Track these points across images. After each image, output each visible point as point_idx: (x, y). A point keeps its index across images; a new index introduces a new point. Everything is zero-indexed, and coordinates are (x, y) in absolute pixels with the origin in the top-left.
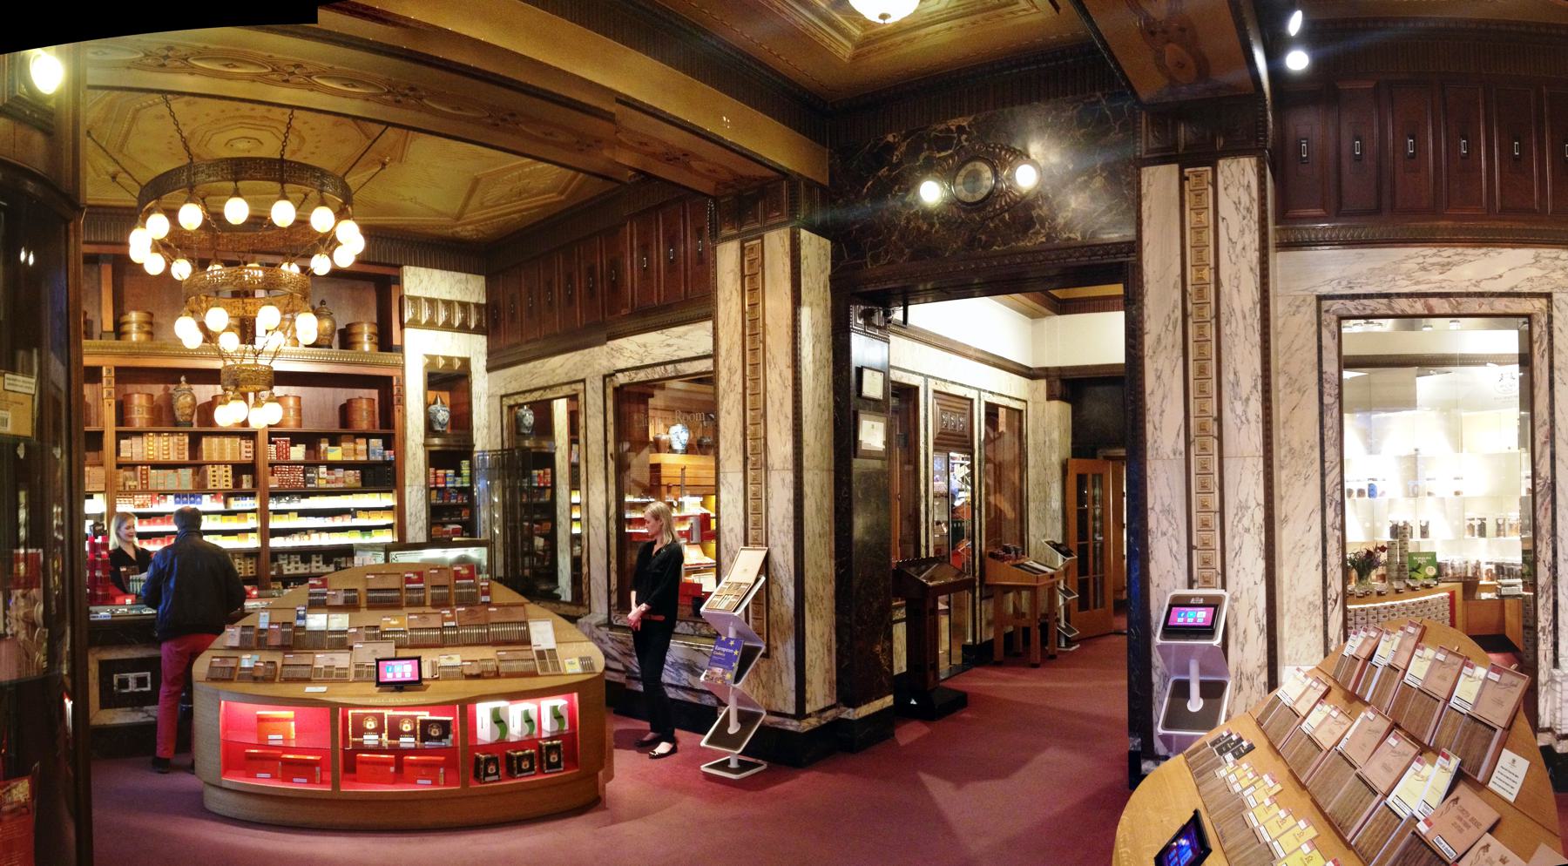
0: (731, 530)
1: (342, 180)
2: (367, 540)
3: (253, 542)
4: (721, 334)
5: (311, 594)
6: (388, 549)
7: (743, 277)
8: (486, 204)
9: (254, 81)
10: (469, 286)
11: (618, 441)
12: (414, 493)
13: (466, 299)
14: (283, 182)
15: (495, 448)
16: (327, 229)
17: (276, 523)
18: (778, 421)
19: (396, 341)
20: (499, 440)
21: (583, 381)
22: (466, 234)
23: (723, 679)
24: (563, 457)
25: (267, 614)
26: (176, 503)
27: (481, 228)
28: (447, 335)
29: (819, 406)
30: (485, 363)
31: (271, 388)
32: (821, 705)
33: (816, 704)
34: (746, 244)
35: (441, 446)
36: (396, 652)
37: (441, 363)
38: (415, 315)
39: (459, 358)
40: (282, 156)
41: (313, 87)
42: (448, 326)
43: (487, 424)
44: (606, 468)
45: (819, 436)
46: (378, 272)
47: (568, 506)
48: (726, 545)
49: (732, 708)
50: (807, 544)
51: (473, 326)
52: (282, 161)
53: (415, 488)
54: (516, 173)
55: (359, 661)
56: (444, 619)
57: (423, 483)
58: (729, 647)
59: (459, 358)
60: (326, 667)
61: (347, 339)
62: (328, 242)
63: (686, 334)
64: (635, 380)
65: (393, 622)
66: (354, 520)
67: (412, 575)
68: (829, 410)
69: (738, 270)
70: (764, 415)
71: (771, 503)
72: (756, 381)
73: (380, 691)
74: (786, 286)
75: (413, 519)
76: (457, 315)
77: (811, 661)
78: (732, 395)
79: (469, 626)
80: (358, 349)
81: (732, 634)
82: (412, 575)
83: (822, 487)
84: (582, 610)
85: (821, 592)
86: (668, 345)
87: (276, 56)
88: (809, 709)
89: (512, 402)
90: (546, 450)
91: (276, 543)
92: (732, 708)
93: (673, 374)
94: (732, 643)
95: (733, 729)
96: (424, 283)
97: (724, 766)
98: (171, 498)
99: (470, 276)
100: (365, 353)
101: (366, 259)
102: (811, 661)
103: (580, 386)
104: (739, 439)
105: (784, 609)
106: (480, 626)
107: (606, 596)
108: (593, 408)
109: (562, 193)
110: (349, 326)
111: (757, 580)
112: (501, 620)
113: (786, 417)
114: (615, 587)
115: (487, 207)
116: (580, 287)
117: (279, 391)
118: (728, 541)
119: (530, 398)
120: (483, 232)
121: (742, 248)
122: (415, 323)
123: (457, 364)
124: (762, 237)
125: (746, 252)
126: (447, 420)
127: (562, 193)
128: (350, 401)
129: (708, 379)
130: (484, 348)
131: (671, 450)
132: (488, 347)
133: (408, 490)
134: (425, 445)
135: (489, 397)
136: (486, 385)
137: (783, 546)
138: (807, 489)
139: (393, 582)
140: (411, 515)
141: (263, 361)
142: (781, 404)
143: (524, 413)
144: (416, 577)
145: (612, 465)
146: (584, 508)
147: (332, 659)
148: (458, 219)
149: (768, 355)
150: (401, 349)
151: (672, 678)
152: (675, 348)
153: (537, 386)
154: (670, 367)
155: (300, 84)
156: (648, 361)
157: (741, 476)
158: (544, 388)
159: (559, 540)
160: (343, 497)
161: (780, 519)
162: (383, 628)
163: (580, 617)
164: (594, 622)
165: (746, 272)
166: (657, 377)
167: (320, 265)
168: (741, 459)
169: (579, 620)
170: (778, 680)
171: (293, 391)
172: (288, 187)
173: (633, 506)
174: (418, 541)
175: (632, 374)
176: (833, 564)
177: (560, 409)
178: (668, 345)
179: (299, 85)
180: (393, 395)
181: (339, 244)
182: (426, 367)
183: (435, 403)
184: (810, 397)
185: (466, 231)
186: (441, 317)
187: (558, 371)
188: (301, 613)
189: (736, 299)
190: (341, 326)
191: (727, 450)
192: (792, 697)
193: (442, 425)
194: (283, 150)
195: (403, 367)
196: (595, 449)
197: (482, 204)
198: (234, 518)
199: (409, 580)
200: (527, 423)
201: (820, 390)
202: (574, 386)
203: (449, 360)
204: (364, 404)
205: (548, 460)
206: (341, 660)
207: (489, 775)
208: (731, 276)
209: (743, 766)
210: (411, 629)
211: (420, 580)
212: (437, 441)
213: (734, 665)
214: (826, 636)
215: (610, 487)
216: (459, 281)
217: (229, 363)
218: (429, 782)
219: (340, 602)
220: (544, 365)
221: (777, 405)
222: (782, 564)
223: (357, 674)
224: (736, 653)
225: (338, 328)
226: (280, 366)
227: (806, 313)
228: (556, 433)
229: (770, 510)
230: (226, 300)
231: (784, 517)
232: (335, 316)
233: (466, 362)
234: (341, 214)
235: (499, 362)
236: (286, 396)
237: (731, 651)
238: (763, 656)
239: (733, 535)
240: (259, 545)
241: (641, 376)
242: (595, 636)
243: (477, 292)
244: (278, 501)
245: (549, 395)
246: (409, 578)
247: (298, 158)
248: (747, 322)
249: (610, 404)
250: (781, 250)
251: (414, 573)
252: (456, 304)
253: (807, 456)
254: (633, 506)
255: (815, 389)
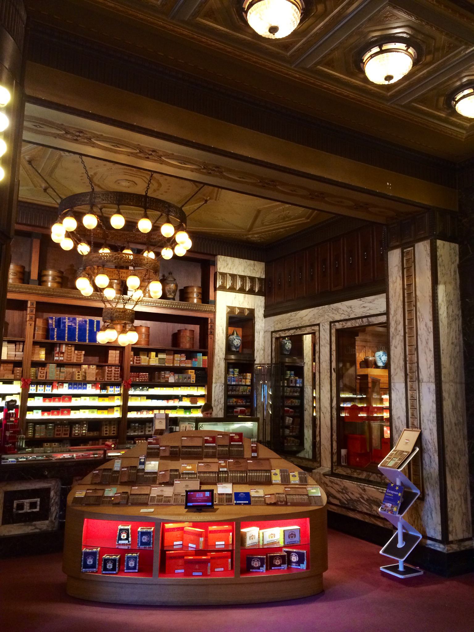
0: (399, 418)
1: (180, 209)
2: (188, 415)
3: (117, 414)
4: (391, 302)
5: (148, 448)
6: (197, 420)
7: (403, 269)
8: (265, 223)
9: (129, 156)
10: (256, 268)
11: (338, 361)
12: (217, 388)
13: (253, 275)
14: (146, 208)
15: (267, 362)
16: (170, 235)
17: (132, 403)
18: (425, 353)
19: (211, 298)
20: (270, 358)
21: (318, 325)
22: (254, 239)
23: (392, 511)
24: (309, 369)
25: (120, 461)
26: (69, 388)
27: (262, 236)
28: (241, 296)
29: (452, 343)
30: (263, 313)
31: (133, 322)
32: (460, 536)
33: (456, 535)
34: (405, 250)
35: (235, 360)
36: (200, 487)
37: (237, 311)
38: (223, 283)
39: (248, 309)
40: (146, 194)
41: (162, 162)
42: (242, 290)
43: (263, 348)
44: (331, 377)
45: (452, 363)
46: (203, 258)
47: (311, 399)
48: (396, 427)
49: (400, 532)
50: (446, 429)
51: (257, 290)
52: (146, 196)
53: (218, 384)
54: (281, 208)
55: (176, 492)
56: (220, 466)
57: (223, 382)
58: (395, 491)
59: (248, 309)
60: (158, 496)
61: (184, 295)
62: (171, 242)
63: (374, 300)
64: (345, 327)
65: (188, 467)
66: (180, 402)
67: (208, 438)
68: (460, 346)
69: (400, 265)
70: (417, 349)
71: (422, 402)
72: (411, 329)
73: (187, 512)
74: (428, 274)
75: (216, 403)
76: (247, 284)
77: (452, 505)
78: (398, 337)
79: (236, 471)
80: (190, 301)
81: (398, 483)
82: (208, 438)
83: (456, 393)
84: (316, 464)
85: (458, 461)
86: (364, 307)
87: (141, 145)
88: (451, 538)
89: (278, 336)
90: (298, 365)
91: (131, 415)
92: (400, 532)
93: (367, 324)
94: (397, 488)
95: (400, 545)
96: (229, 266)
97: (395, 569)
98: (66, 385)
99: (256, 262)
100: (195, 304)
101: (193, 250)
102: (452, 505)
103: (316, 328)
104: (402, 363)
105: (432, 470)
106: (241, 472)
107: (330, 456)
108: (323, 341)
109: (308, 218)
110: (186, 288)
111: (414, 450)
112: (256, 468)
113: (430, 350)
114: (336, 451)
115: (266, 225)
116: (318, 270)
117: (137, 323)
118: (397, 424)
119: (288, 333)
120: (264, 238)
121: (403, 253)
122: (223, 288)
123: (247, 313)
124: (414, 246)
125: (405, 255)
126: (239, 344)
127: (308, 218)
128: (179, 331)
129: (386, 325)
130: (263, 304)
131: (377, 367)
132: (265, 303)
133: (214, 385)
134: (225, 359)
135: (265, 332)
136: (263, 325)
137: (430, 430)
138: (445, 395)
139: (198, 442)
140: (215, 401)
141: (129, 307)
142: (427, 343)
143: (286, 342)
144: (211, 439)
145: (334, 375)
146: (318, 400)
147: (162, 491)
148: (250, 230)
149: (418, 314)
150: (214, 303)
151: (367, 509)
152: (368, 308)
153: (292, 327)
154: (365, 320)
155: (155, 160)
156: (352, 316)
157: (404, 385)
158: (296, 328)
159: (305, 419)
160: (175, 388)
161: (428, 413)
162: (181, 471)
163: (314, 469)
164: (322, 472)
165: (405, 266)
166: (357, 325)
167: (167, 254)
168: (404, 375)
169: (314, 471)
170: (430, 516)
171: (149, 323)
172: (149, 212)
173: (346, 400)
174: (218, 417)
175: (344, 323)
176: (466, 443)
177: (307, 340)
178: (364, 307)
179: (155, 161)
180: (208, 329)
181: (177, 244)
182: (228, 313)
183: (233, 334)
184: (446, 338)
185: (254, 237)
186: (239, 285)
187: (304, 318)
188: (142, 460)
189: (399, 281)
190: (181, 287)
191: (395, 369)
192: (439, 528)
193: (236, 347)
194: (147, 191)
195: (214, 313)
196: (325, 365)
197: (263, 223)
198: (106, 399)
199: (207, 441)
200: (287, 348)
201: (453, 334)
202: (313, 328)
203: (242, 310)
204: (188, 334)
205: (299, 372)
206: (168, 491)
207: (121, 539)
208: (396, 269)
209: (407, 570)
210: (199, 472)
211: (214, 442)
212: (233, 357)
213: (398, 502)
214: (463, 491)
215: (333, 388)
216: (250, 265)
217: (108, 306)
218: (200, 574)
219: (167, 454)
220: (296, 314)
221: (424, 343)
222: (431, 442)
223: (176, 500)
224: (400, 494)
225: (179, 288)
226: (139, 308)
227: (441, 289)
228: (305, 354)
229: (422, 407)
230: (112, 270)
231: (430, 411)
232: (178, 281)
233: (252, 311)
234: (178, 228)
235: (272, 312)
236: (141, 326)
237: (396, 493)
238: (418, 498)
239: (399, 421)
240: (121, 416)
241: (349, 325)
242: (323, 481)
243: (260, 271)
244: (135, 389)
245: (299, 332)
246: (207, 440)
247: (154, 195)
248: (406, 295)
249: (334, 339)
250: (425, 253)
251: (210, 437)
252: (247, 278)
253: (445, 374)
254: (346, 400)
255: (449, 334)
